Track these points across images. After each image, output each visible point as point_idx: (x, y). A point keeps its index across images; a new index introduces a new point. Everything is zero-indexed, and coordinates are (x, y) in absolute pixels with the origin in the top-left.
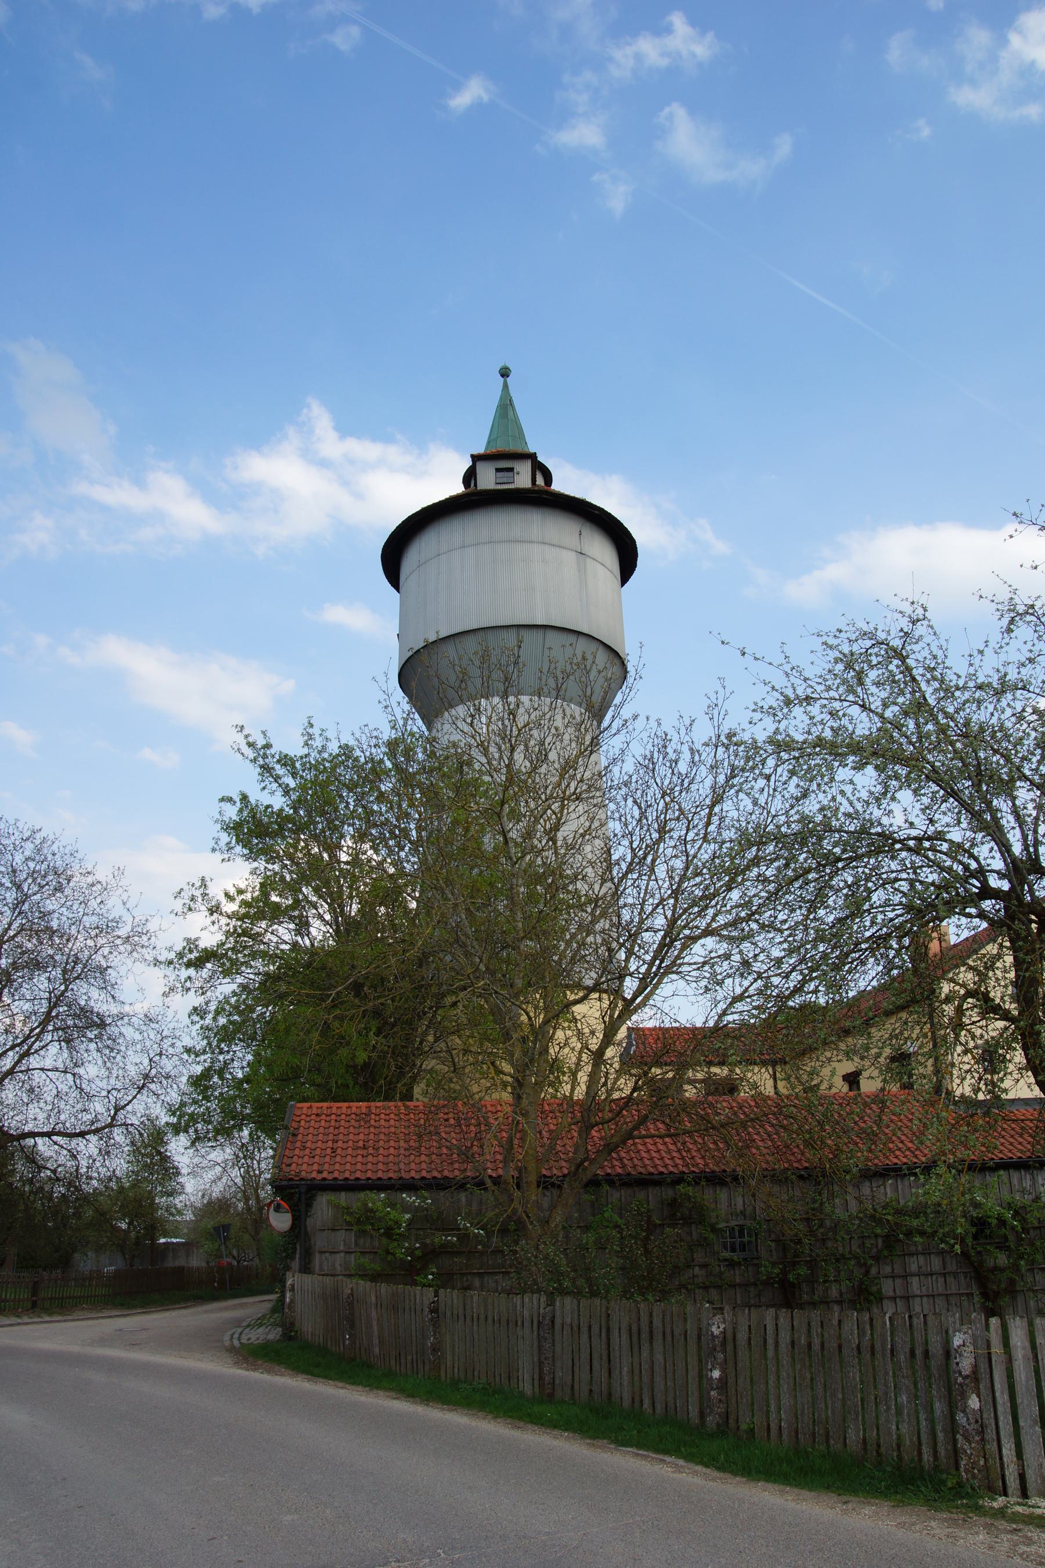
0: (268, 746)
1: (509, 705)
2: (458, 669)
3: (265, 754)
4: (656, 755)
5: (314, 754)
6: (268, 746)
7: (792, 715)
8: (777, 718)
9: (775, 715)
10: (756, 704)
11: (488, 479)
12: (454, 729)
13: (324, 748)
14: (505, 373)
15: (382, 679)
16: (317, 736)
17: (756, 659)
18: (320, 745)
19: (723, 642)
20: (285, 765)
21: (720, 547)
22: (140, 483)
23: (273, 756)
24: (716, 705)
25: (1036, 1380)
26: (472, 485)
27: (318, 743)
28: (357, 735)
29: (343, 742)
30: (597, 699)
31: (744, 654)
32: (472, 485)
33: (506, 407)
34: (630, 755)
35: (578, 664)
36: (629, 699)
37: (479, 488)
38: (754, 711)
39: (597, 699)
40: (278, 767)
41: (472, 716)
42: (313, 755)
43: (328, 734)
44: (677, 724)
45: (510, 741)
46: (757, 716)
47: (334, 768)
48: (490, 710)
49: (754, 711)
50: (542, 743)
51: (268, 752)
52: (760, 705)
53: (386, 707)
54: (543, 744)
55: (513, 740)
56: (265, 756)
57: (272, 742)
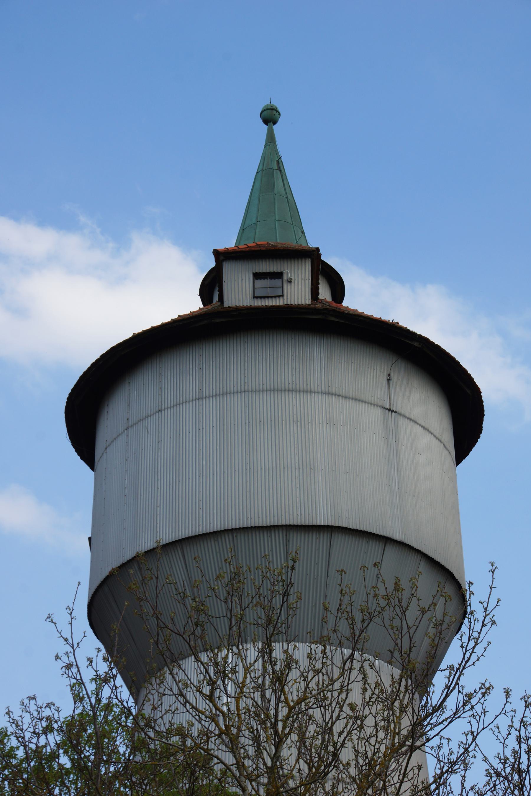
4: (524, 758)
11: (241, 290)
14: (270, 117)
15: (62, 618)
30: (419, 656)
33: (271, 173)
35: (387, 597)
36: (474, 658)
37: (226, 304)
41: (212, 683)
45: (274, 726)
50: (327, 730)
53: (69, 666)
55: (280, 725)
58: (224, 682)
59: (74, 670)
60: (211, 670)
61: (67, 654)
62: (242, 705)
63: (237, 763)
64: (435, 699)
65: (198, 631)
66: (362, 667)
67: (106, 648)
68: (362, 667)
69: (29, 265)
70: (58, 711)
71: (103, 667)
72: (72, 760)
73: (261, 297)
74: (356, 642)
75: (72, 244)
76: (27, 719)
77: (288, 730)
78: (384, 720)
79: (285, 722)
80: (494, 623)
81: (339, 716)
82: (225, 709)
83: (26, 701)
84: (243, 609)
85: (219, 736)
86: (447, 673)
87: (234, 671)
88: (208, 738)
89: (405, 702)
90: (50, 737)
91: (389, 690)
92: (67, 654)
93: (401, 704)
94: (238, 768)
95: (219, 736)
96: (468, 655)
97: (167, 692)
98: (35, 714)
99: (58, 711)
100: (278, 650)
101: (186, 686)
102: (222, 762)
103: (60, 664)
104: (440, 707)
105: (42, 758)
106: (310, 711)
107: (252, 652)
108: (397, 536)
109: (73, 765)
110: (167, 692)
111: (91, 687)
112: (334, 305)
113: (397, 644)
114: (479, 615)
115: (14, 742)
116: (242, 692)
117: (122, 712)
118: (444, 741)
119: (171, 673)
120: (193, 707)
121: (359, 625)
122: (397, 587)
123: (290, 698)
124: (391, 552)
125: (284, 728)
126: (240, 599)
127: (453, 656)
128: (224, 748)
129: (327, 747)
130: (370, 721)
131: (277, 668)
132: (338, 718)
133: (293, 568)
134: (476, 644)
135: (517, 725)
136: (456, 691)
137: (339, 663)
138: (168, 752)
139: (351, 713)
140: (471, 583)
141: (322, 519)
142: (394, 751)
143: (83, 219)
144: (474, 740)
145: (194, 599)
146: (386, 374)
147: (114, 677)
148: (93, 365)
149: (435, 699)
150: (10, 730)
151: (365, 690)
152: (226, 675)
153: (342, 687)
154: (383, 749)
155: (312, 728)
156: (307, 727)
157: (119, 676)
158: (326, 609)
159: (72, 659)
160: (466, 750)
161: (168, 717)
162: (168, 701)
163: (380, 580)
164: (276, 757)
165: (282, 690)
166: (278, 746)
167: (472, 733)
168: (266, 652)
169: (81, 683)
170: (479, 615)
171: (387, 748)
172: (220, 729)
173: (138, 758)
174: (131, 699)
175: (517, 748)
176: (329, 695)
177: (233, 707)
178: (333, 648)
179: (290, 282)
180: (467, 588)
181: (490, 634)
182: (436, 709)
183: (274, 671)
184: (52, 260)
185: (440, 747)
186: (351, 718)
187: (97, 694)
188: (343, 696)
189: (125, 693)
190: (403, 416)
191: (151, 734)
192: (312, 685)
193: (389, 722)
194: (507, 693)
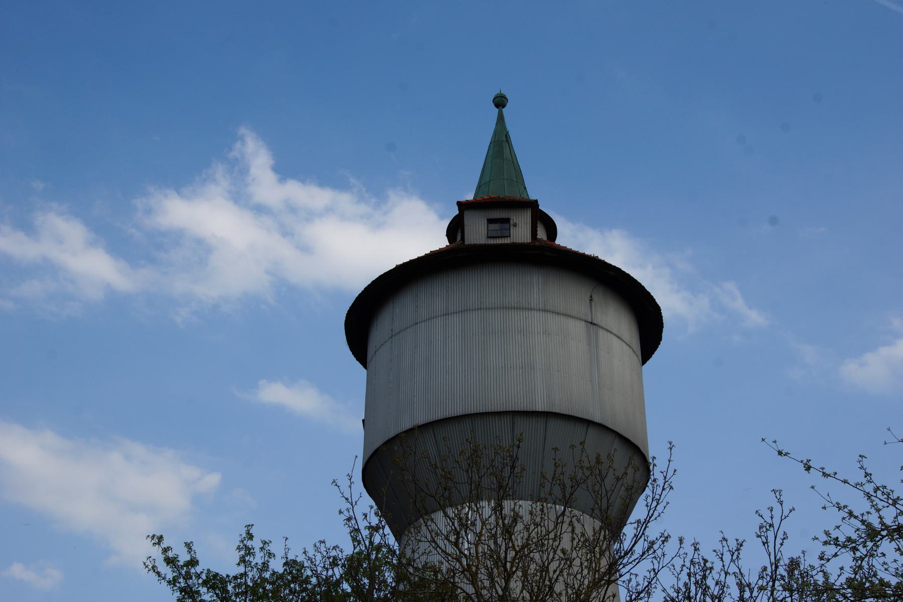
0: (193, 562)
1: (503, 519)
2: (439, 471)
3: (188, 573)
4: (693, 588)
5: (253, 574)
6: (193, 562)
7: (879, 551)
8: (858, 554)
9: (855, 549)
10: (827, 533)
11: (477, 232)
12: (436, 545)
13: (265, 566)
14: (500, 102)
15: (344, 483)
16: (257, 550)
17: (825, 475)
18: (260, 562)
19: (780, 453)
20: (213, 587)
21: (755, 318)
22: (26, 227)
23: (198, 576)
24: (771, 525)
25: (538, 412)
26: (459, 238)
27: (258, 559)
28: (310, 555)
29: (291, 557)
30: (614, 513)
31: (808, 468)
32: (459, 238)
33: (501, 143)
34: (659, 587)
35: (590, 468)
36: (656, 514)
37: (466, 243)
38: (825, 543)
39: (614, 513)
40: (203, 590)
41: (458, 533)
42: (250, 575)
43: (272, 548)
44: (719, 547)
45: (505, 566)
46: (831, 550)
47: (276, 591)
48: (479, 524)
49: (825, 543)
50: (544, 569)
51: (193, 571)
52: (834, 536)
53: (349, 519)
54: (547, 571)
55: (508, 565)
56: (188, 576)
57: (199, 557)
58: (466, 532)
59: (353, 522)
60: (456, 524)
61: (348, 510)
62: (480, 549)
63: (476, 592)
64: (626, 545)
65: (447, 493)
66: (571, 521)
67: (376, 504)
68: (571, 521)
69: (311, 216)
70: (341, 551)
71: (375, 521)
72: (352, 587)
73: (493, 237)
74: (567, 502)
75: (345, 200)
76: (319, 557)
77: (514, 569)
78: (587, 560)
79: (512, 563)
80: (671, 488)
81: (553, 558)
82: (466, 552)
83: (318, 544)
84: (480, 478)
85: (463, 572)
86: (636, 525)
87: (473, 524)
88: (454, 574)
89: (604, 547)
90: (336, 569)
91: (592, 538)
92: (348, 510)
93: (600, 549)
94: (477, 597)
95: (463, 572)
96: (651, 512)
97: (423, 539)
98: (325, 554)
99: (341, 551)
100: (507, 505)
101: (437, 534)
102: (464, 592)
103: (343, 517)
104: (631, 551)
105: (332, 585)
106: (532, 555)
107: (487, 508)
108: (597, 419)
109: (353, 591)
110: (423, 539)
111: (365, 533)
112: (549, 243)
113: (596, 503)
114: (661, 482)
115: (309, 573)
116: (479, 540)
117: (388, 552)
118: (633, 577)
119: (426, 525)
120: (442, 551)
121: (568, 490)
122: (598, 461)
123: (516, 544)
124: (592, 433)
125: (512, 567)
126: (478, 470)
127: (639, 512)
128: (465, 580)
129: (544, 581)
130: (577, 562)
131: (506, 522)
132: (552, 560)
133: (518, 447)
134: (658, 504)
135: (688, 564)
136: (642, 539)
137: (553, 518)
138: (423, 583)
139: (562, 556)
140: (654, 458)
141: (540, 406)
142: (595, 585)
143: (353, 180)
144: (656, 574)
145: (443, 470)
146: (588, 298)
147: (383, 527)
148: (366, 289)
149: (626, 545)
150: (306, 564)
151: (573, 539)
152: (467, 527)
153: (556, 536)
154: (586, 582)
155: (533, 567)
156: (529, 566)
157: (387, 527)
158: (544, 477)
159: (351, 513)
160: (650, 583)
161: (423, 558)
162: (424, 546)
163: (584, 454)
164: (506, 589)
165: (510, 539)
166: (507, 582)
167: (654, 570)
168: (498, 509)
169: (358, 530)
170: (661, 482)
171: (589, 582)
172: (463, 567)
173: (401, 587)
174: (397, 544)
175: (687, 581)
176: (546, 542)
177: (473, 551)
178: (549, 505)
179: (515, 225)
180: (651, 461)
181: (668, 496)
182: (626, 554)
183: (504, 524)
184: (329, 211)
185: (630, 581)
186: (562, 559)
187: (370, 538)
188: (556, 543)
189: (391, 540)
190: (602, 328)
191: (411, 570)
192: (533, 534)
193: (591, 562)
194: (681, 541)
